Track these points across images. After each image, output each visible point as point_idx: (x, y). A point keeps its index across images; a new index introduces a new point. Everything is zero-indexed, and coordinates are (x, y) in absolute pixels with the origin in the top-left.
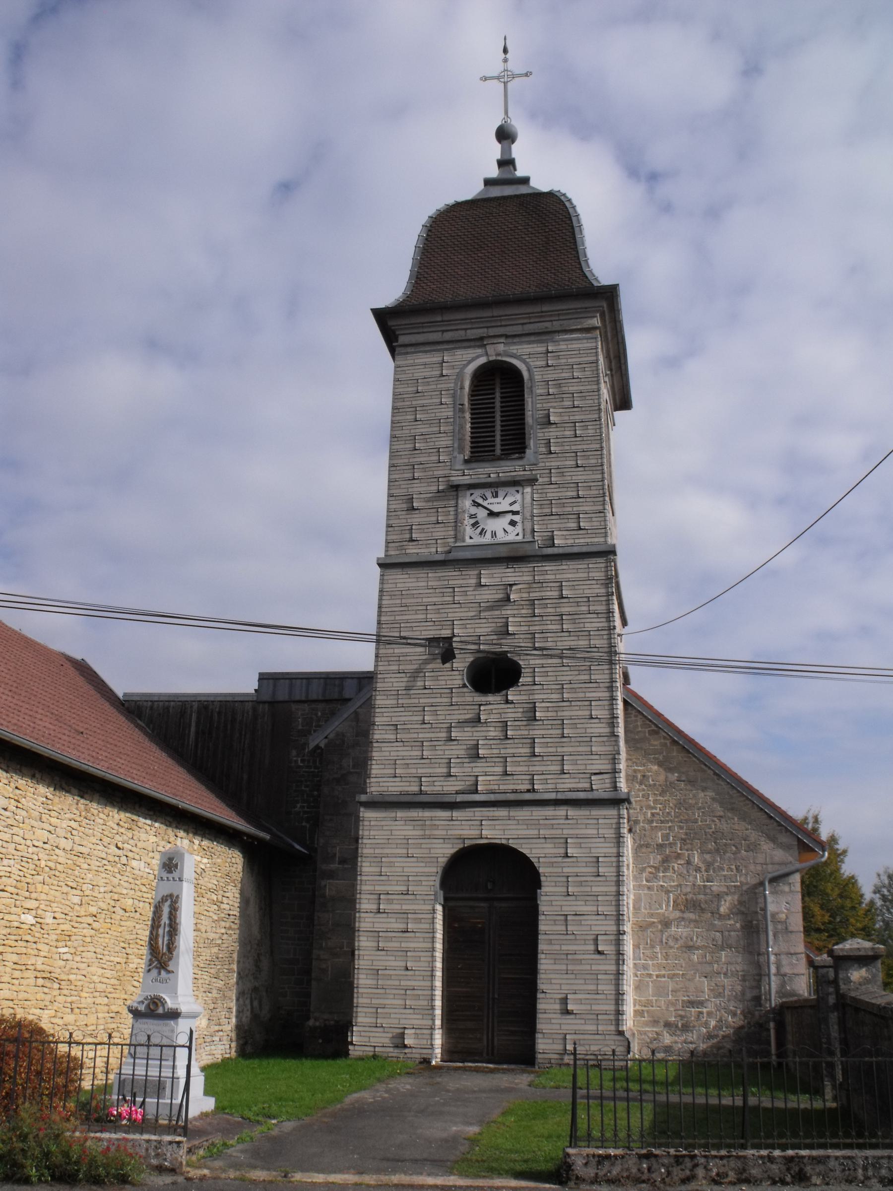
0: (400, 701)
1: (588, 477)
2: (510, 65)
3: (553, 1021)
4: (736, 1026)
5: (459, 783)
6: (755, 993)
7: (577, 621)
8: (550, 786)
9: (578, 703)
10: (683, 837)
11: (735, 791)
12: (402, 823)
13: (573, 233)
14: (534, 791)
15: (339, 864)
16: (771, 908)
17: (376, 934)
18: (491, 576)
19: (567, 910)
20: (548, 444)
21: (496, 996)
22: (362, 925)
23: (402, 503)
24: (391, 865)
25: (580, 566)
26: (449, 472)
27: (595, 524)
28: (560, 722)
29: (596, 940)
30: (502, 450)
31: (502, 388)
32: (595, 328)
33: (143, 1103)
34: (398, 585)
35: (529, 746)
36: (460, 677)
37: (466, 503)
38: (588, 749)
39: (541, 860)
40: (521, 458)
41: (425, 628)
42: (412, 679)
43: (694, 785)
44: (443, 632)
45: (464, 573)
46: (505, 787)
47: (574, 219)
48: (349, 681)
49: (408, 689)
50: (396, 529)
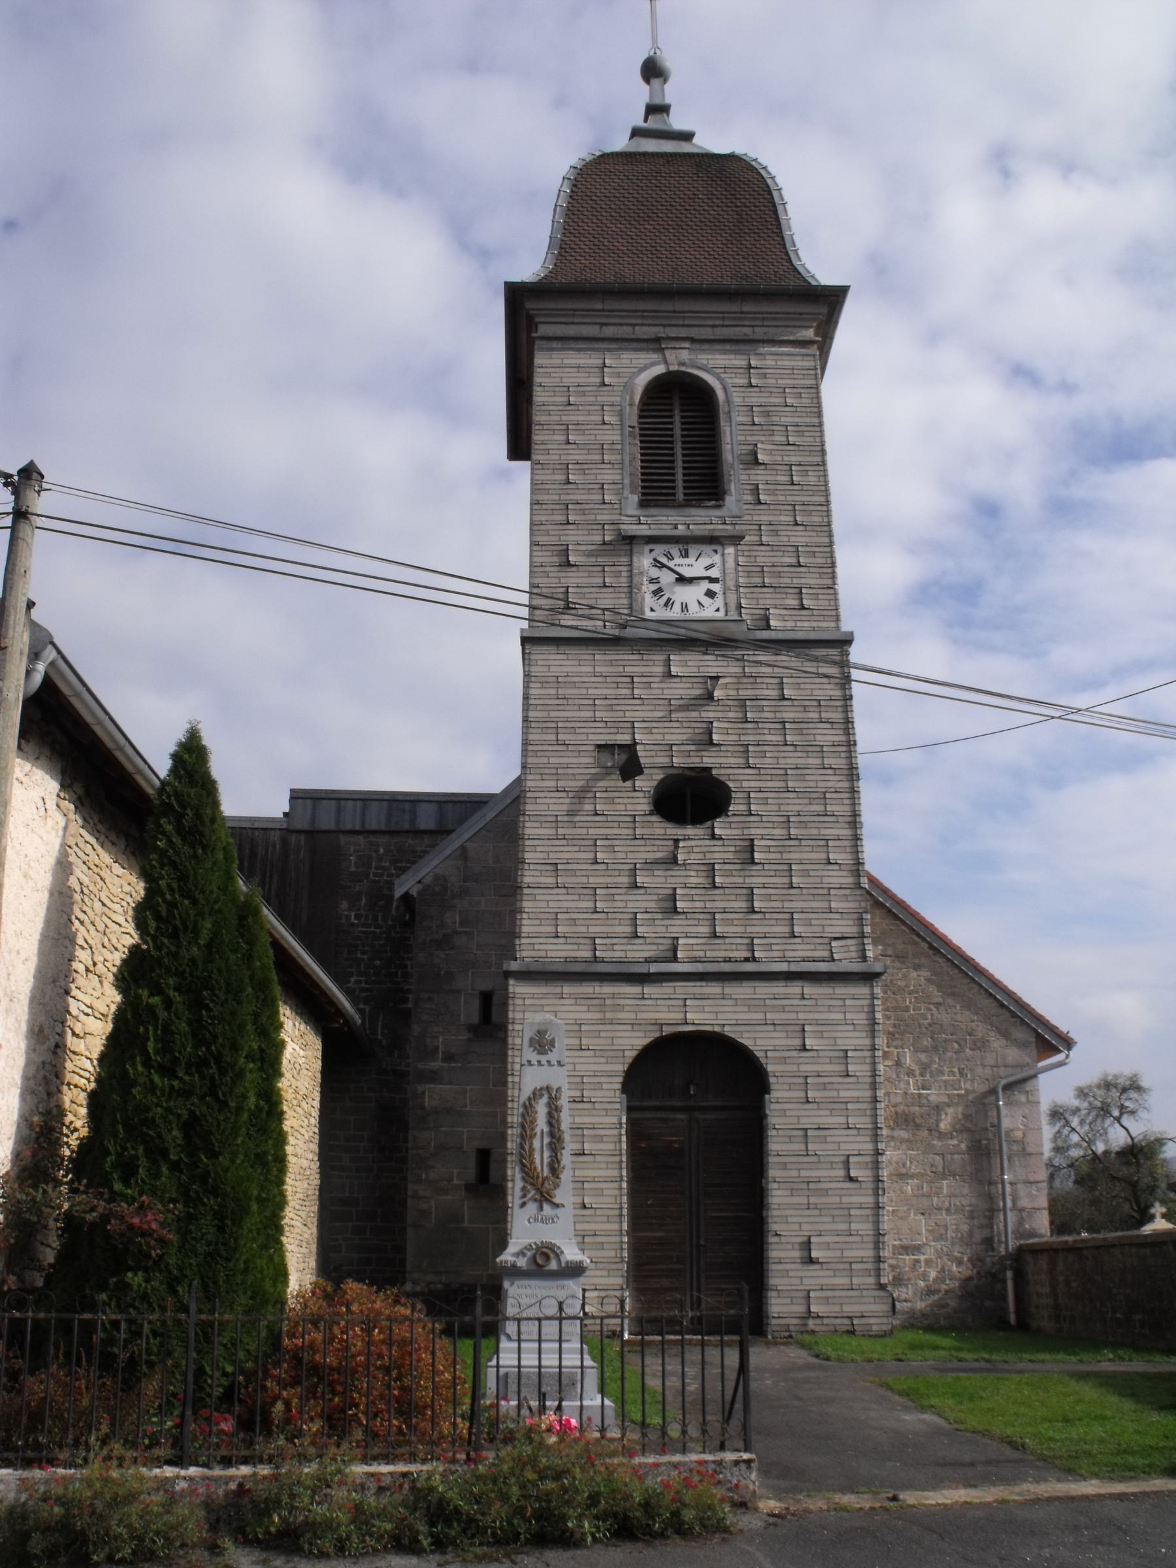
0: (560, 831)
1: (812, 540)
3: (791, 1274)
4: (963, 1277)
5: (649, 947)
6: (986, 1233)
7: (805, 732)
8: (776, 954)
10: (891, 1029)
11: (956, 971)
12: (572, 1001)
13: (776, 212)
14: (754, 959)
16: (1006, 1123)
18: (685, 664)
19: (806, 1122)
20: (756, 490)
21: (702, 1242)
26: (618, 517)
30: (685, 494)
31: (682, 411)
32: (812, 342)
33: (559, 1408)
35: (745, 898)
36: (645, 800)
37: (644, 561)
38: (826, 904)
39: (769, 1054)
40: (719, 507)
41: (593, 731)
42: (577, 801)
43: (903, 962)
44: (619, 737)
46: (715, 954)
47: (775, 194)
48: (425, 804)
49: (571, 814)
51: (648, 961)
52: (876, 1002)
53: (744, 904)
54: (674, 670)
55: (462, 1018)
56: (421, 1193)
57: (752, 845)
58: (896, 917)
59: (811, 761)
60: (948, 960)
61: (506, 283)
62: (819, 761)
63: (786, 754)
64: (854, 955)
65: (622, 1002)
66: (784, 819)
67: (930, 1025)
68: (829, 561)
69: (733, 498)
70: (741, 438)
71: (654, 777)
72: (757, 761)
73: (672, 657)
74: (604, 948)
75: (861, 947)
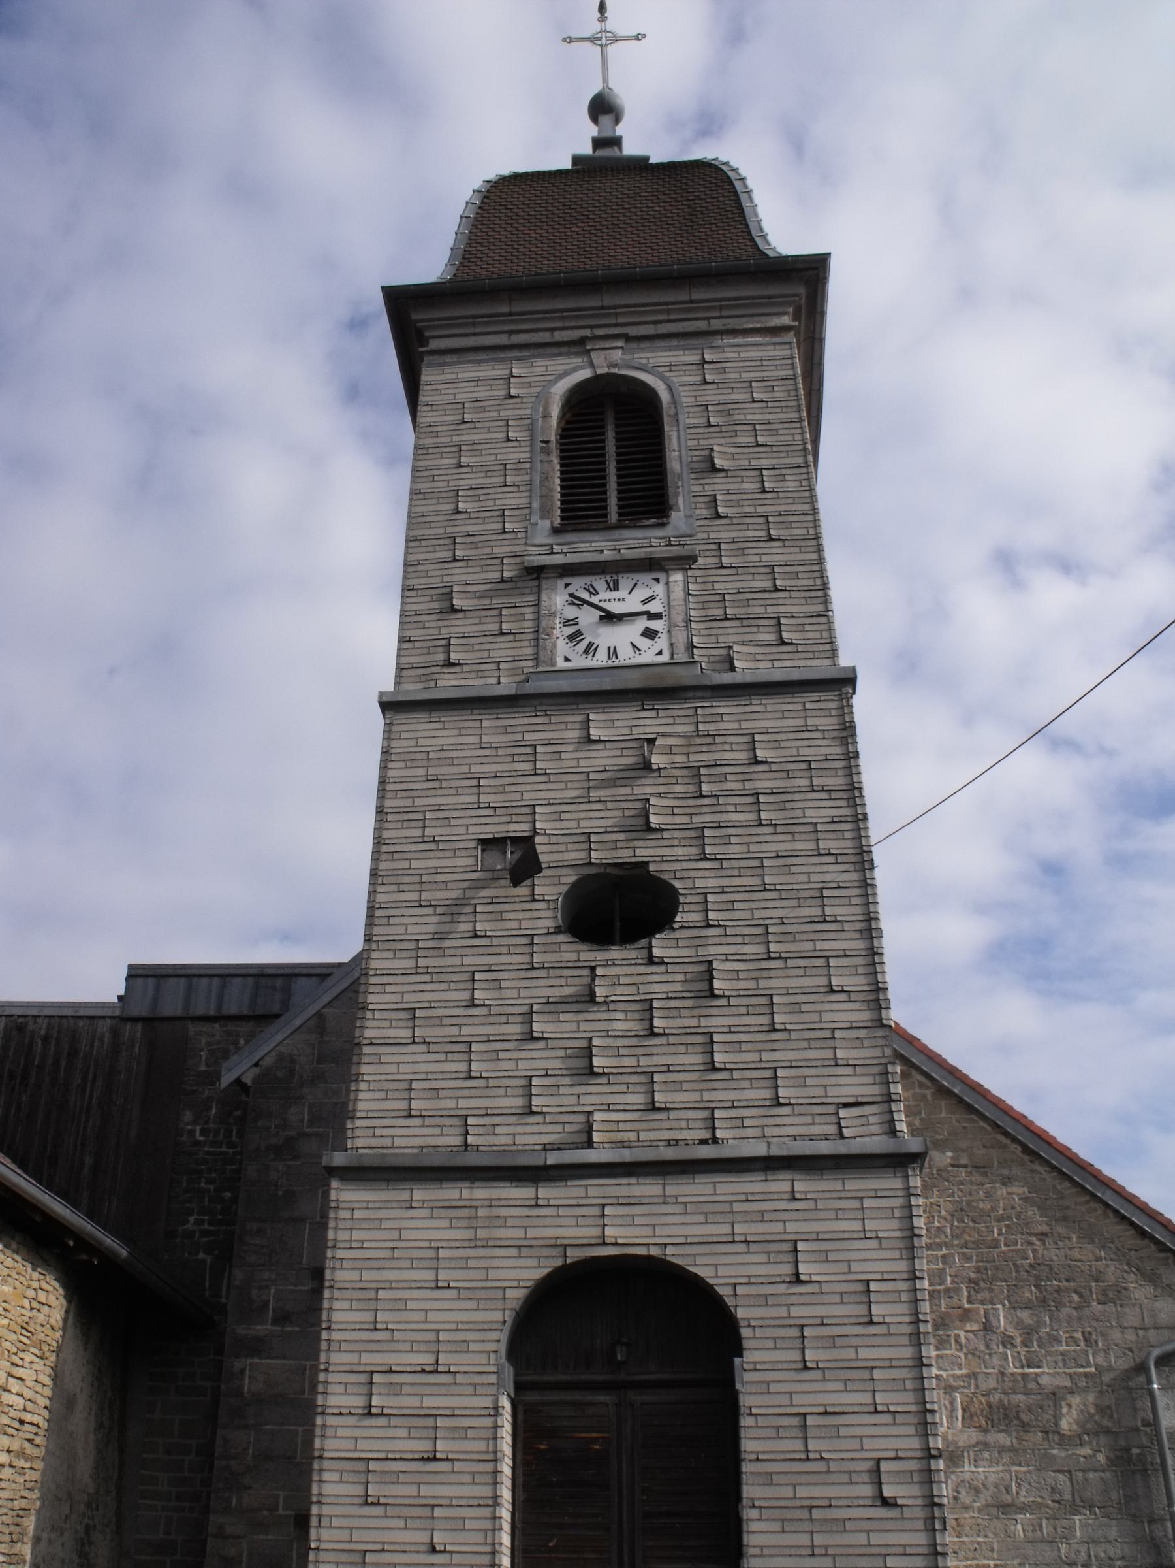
0: (422, 962)
2: (610, 25)
5: (550, 1128)
7: (788, 805)
9: (802, 963)
10: (973, 1275)
11: (1067, 1184)
15: (275, 1321)
17: (361, 1466)
19: (803, 1402)
22: (330, 1444)
23: (429, 600)
24: (399, 1306)
25: (790, 707)
26: (522, 548)
27: (811, 635)
28: (764, 1000)
29: (876, 1473)
32: (786, 329)
34: (421, 742)
36: (549, 913)
37: (557, 599)
38: (829, 1054)
40: (663, 525)
41: (475, 821)
42: (448, 919)
43: (985, 1174)
45: (553, 719)
48: (303, 980)
49: (439, 937)
50: (417, 645)
51: (545, 1148)
52: (913, 1201)
53: (699, 1059)
54: (594, 733)
55: (304, 1260)
56: (229, 1530)
57: (710, 971)
58: (970, 1109)
59: (800, 846)
60: (1054, 1168)
61: (383, 288)
62: (811, 845)
63: (762, 838)
64: (875, 1129)
65: (504, 1212)
66: (760, 930)
67: (1031, 1266)
68: (818, 582)
69: (681, 514)
70: (690, 443)
71: (563, 880)
72: (716, 850)
73: (592, 717)
74: (481, 1130)
75: (887, 1117)
